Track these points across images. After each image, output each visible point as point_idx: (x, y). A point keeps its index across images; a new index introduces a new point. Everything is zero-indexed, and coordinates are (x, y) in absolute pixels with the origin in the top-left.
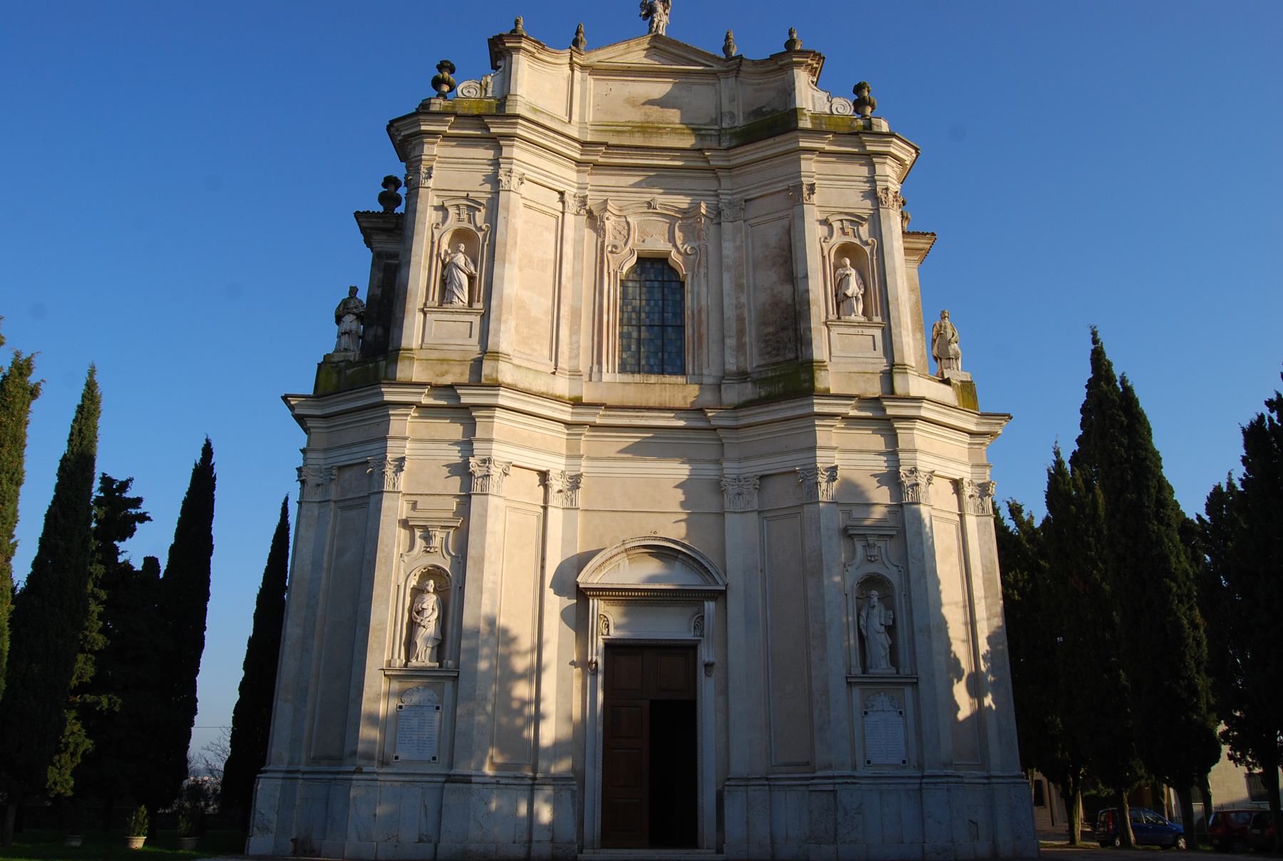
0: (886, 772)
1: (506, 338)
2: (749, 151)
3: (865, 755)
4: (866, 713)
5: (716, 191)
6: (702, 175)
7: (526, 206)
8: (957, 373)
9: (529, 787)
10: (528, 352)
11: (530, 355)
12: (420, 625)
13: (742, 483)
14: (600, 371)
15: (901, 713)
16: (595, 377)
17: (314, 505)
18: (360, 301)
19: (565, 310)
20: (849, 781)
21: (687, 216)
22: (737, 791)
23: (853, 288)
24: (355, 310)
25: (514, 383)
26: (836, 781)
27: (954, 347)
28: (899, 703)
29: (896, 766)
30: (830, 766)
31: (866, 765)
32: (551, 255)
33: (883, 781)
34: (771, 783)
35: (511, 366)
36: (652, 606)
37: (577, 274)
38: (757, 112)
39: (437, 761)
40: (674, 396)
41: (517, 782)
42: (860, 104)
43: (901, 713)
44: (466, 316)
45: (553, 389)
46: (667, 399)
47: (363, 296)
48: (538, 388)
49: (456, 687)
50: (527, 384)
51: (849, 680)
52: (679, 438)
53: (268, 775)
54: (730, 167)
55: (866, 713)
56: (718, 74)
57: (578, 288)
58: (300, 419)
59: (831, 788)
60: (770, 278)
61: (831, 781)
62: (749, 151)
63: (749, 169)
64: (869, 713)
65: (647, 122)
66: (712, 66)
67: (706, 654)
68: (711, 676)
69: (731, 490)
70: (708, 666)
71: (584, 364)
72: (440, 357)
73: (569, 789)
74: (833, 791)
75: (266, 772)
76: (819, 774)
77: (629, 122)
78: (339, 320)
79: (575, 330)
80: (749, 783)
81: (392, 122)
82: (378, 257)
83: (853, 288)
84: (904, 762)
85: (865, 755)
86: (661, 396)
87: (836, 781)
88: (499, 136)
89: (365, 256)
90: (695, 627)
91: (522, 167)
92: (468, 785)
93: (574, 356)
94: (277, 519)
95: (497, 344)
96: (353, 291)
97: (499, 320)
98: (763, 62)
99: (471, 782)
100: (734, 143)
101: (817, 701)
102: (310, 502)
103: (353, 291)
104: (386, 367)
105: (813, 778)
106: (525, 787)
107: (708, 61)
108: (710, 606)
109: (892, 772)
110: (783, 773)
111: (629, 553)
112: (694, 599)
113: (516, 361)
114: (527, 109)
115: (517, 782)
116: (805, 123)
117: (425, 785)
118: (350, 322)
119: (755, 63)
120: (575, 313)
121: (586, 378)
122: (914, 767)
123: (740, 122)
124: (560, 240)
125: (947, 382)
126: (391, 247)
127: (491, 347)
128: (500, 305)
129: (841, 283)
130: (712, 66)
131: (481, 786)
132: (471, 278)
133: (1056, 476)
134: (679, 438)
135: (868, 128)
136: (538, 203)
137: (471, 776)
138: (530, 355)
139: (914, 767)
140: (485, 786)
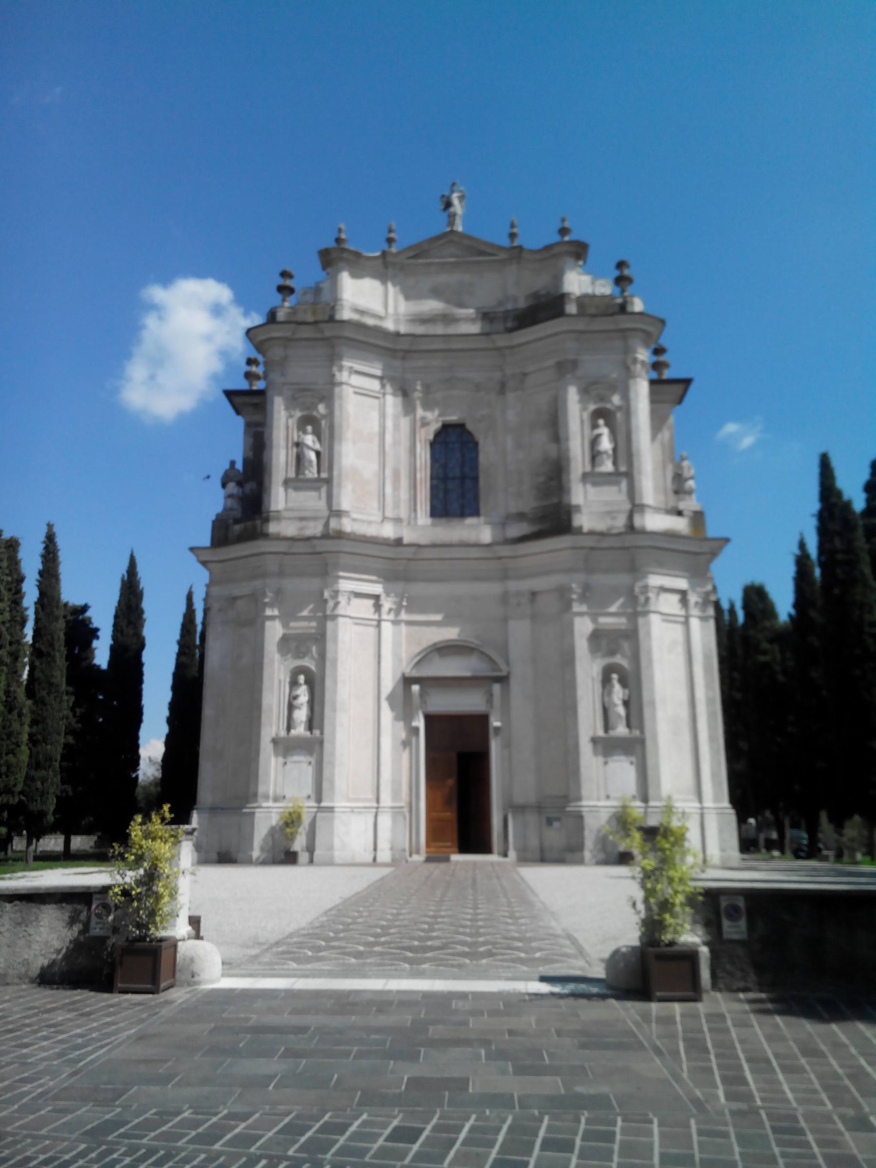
1: (345, 501)
7: (356, 393)
8: (690, 504)
9: (374, 810)
12: (341, 384)
14: (416, 518)
16: (412, 522)
18: (238, 471)
19: (389, 472)
23: (606, 444)
27: (691, 483)
32: (376, 429)
37: (396, 443)
38: (536, 295)
42: (622, 281)
47: (239, 466)
57: (397, 455)
58: (204, 563)
60: (541, 438)
70: (497, 729)
71: (403, 512)
78: (224, 485)
79: (396, 487)
82: (248, 425)
83: (606, 444)
89: (239, 422)
93: (397, 506)
94: (182, 608)
95: (339, 504)
96: (233, 463)
97: (340, 485)
98: (538, 251)
103: (233, 463)
108: (497, 688)
113: (354, 515)
116: (571, 308)
118: (232, 487)
119: (532, 252)
120: (396, 474)
121: (405, 523)
123: (522, 304)
124: (383, 416)
125: (680, 513)
126: (257, 418)
127: (335, 508)
128: (340, 475)
129: (595, 441)
132: (318, 454)
133: (802, 562)
135: (623, 309)
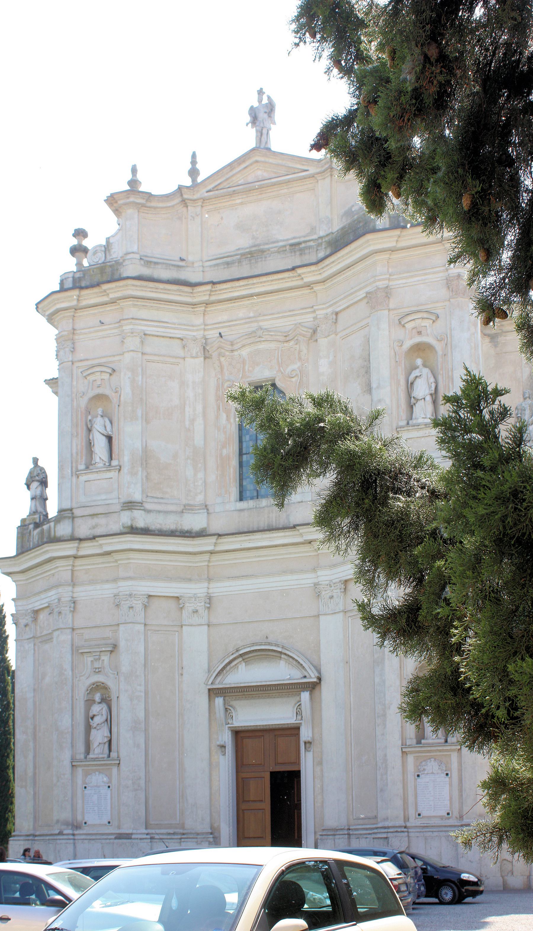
0: (432, 822)
2: (333, 262)
3: (416, 810)
4: (418, 776)
5: (312, 307)
6: (277, 297)
10: (160, 495)
11: (162, 498)
13: (333, 588)
15: (447, 774)
17: (25, 641)
20: (399, 830)
21: (288, 339)
22: (327, 839)
24: (37, 478)
25: (146, 526)
26: (389, 830)
28: (446, 767)
29: (441, 817)
30: (386, 819)
31: (417, 816)
33: (428, 830)
34: (351, 833)
35: (143, 512)
36: (248, 699)
39: (111, 824)
40: (279, 516)
41: (169, 837)
43: (447, 774)
44: (108, 473)
45: (181, 525)
46: (274, 520)
48: (168, 527)
49: (119, 770)
50: (158, 525)
51: (403, 750)
52: (302, 552)
53: (16, 838)
54: (194, 304)
55: (418, 776)
56: (315, 176)
59: (385, 835)
61: (386, 830)
62: (333, 262)
63: (338, 279)
64: (421, 776)
65: (255, 246)
66: (207, 192)
67: (305, 734)
68: (310, 751)
69: (325, 594)
72: (91, 513)
73: (207, 841)
74: (387, 838)
75: (14, 836)
76: (380, 825)
77: (239, 249)
78: (29, 488)
80: (336, 833)
81: (37, 305)
84: (448, 814)
85: (416, 810)
86: (268, 517)
87: (389, 830)
88: (118, 300)
90: (297, 713)
91: (140, 325)
92: (129, 841)
99: (131, 838)
100: (328, 252)
101: (380, 768)
102: (22, 640)
104: (55, 527)
105: (377, 828)
106: (176, 841)
107: (303, 165)
108: (305, 696)
109: (439, 822)
110: (360, 825)
111: (244, 657)
112: (282, 691)
114: (142, 265)
115: (169, 837)
117: (104, 841)
122: (456, 818)
130: (207, 192)
131: (139, 841)
134: (302, 552)
136: (159, 355)
137: (132, 834)
138: (162, 498)
139: (456, 818)
140: (142, 841)
